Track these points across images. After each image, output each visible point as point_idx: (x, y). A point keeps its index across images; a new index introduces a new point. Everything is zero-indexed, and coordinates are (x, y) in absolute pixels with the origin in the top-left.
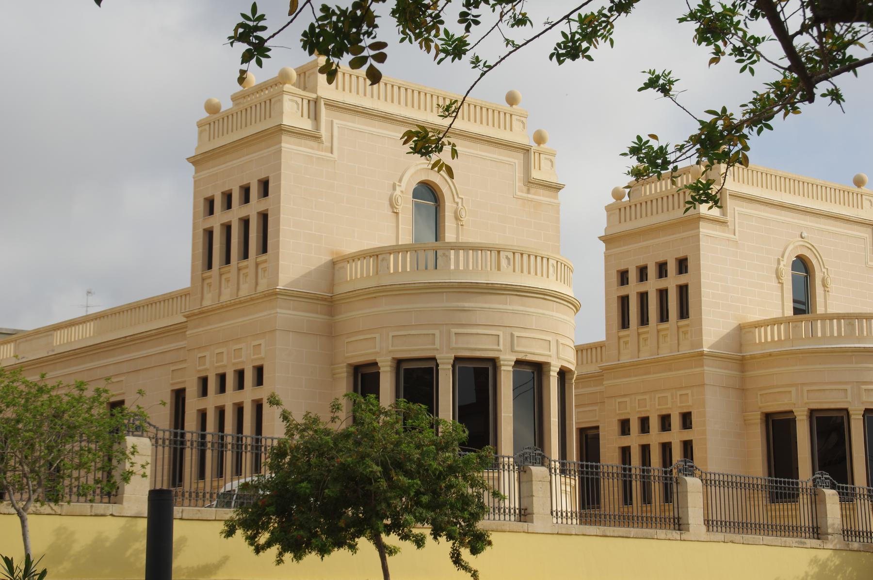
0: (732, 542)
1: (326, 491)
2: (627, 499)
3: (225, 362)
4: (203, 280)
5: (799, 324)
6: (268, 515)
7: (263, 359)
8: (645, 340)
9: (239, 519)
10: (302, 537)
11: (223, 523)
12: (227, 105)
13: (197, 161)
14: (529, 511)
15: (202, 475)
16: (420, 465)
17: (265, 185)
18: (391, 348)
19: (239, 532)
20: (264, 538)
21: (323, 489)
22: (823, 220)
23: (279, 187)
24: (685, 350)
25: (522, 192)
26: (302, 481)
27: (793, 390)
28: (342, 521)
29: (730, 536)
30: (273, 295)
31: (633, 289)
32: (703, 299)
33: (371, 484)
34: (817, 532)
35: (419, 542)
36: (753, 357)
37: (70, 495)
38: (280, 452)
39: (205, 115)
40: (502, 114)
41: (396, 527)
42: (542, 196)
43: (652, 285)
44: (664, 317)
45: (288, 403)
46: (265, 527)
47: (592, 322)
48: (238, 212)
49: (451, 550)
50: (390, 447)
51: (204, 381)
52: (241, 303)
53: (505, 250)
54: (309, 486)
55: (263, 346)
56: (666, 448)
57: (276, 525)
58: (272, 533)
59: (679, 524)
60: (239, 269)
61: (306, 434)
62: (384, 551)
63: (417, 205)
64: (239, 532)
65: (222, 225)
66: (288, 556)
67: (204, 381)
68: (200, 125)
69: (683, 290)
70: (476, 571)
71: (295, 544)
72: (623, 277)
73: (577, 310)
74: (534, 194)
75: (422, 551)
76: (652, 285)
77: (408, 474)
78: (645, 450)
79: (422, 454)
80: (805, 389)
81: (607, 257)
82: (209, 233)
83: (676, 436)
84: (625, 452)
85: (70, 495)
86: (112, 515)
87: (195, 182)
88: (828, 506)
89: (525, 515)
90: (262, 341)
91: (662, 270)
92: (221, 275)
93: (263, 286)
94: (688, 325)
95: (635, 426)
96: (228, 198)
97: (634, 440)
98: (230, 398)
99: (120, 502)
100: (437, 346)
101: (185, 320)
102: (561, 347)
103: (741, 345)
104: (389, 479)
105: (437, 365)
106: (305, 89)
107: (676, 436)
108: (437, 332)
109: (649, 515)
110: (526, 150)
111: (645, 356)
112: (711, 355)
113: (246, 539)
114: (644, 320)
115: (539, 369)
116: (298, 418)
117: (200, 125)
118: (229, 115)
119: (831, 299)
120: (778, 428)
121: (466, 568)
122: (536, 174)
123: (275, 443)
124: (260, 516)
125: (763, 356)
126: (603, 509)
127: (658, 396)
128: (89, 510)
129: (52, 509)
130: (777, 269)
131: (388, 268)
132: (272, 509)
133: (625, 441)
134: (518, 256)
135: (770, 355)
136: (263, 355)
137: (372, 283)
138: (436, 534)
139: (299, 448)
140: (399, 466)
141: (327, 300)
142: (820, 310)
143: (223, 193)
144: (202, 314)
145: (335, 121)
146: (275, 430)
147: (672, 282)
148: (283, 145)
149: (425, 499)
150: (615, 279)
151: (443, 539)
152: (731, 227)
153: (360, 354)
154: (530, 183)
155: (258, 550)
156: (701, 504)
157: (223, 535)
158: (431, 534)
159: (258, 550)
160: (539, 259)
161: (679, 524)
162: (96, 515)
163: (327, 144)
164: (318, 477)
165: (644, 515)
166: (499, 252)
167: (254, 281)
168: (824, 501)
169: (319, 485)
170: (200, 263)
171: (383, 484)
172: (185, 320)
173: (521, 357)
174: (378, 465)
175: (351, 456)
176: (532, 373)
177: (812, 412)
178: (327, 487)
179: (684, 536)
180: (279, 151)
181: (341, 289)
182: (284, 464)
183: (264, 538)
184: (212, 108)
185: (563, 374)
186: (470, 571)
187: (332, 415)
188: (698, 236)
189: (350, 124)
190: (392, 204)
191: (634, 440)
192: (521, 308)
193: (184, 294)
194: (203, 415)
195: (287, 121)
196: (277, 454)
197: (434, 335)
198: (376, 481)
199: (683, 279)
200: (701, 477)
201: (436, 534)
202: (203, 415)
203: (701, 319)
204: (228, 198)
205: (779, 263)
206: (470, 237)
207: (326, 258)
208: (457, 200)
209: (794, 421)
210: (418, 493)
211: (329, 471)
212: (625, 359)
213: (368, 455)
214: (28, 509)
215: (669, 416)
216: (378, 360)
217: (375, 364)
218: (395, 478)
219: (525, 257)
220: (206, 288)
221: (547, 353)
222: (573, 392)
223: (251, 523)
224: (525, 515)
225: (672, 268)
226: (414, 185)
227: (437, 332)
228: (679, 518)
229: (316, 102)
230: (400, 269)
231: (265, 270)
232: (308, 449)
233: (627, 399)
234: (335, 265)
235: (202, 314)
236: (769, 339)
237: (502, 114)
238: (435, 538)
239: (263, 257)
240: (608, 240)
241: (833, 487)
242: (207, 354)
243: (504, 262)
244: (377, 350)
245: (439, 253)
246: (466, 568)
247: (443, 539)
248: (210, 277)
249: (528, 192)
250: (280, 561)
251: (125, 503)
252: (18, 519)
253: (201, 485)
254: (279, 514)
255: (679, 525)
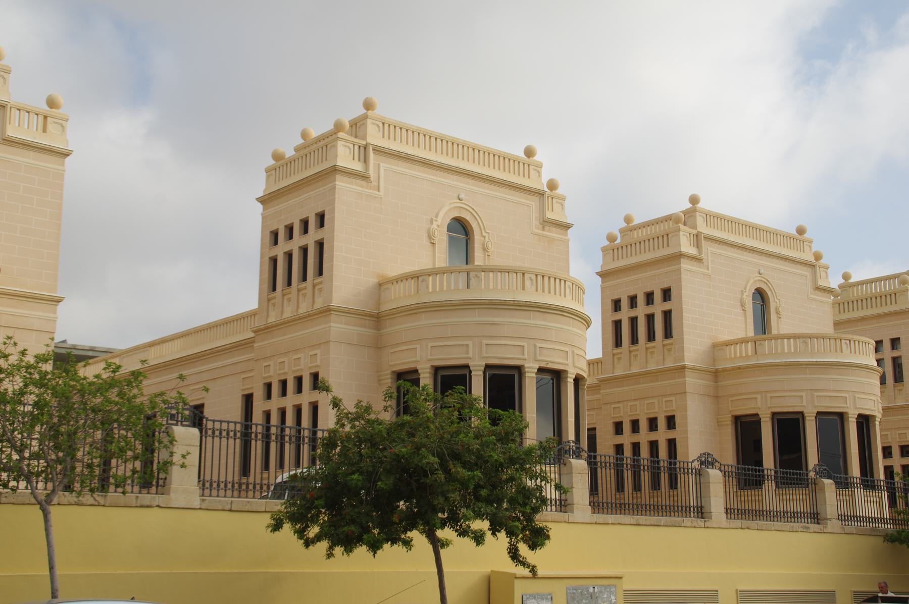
0: (748, 528)
1: (379, 483)
2: (620, 487)
3: (286, 370)
4: (269, 300)
5: (763, 342)
6: (316, 507)
7: (318, 366)
8: (636, 356)
9: (287, 512)
10: (353, 532)
11: (268, 516)
12: (289, 153)
13: (263, 200)
14: (569, 502)
15: (266, 466)
16: (479, 456)
17: (321, 218)
18: (430, 357)
19: (287, 527)
20: (314, 531)
21: (375, 482)
22: (775, 260)
23: (333, 218)
24: (669, 364)
25: (538, 229)
26: (353, 473)
27: (759, 396)
28: (396, 516)
29: (746, 523)
30: (327, 311)
31: (625, 315)
32: (684, 322)
33: (427, 476)
34: (816, 517)
35: (479, 538)
36: (724, 370)
37: (132, 486)
38: (331, 442)
39: (272, 162)
40: (521, 164)
41: (453, 520)
42: (554, 233)
43: (641, 311)
44: (651, 337)
45: (337, 391)
46: (314, 520)
47: (593, 343)
48: (299, 240)
49: (508, 545)
50: (447, 436)
51: (269, 386)
52: (300, 318)
53: (529, 272)
54: (361, 478)
55: (318, 356)
56: (654, 445)
57: (326, 518)
58: (321, 528)
59: (701, 512)
60: (299, 290)
61: (357, 423)
62: (437, 544)
63: (450, 237)
64: (287, 527)
65: (285, 253)
66: (338, 550)
67: (269, 386)
68: (268, 171)
69: (667, 315)
70: (534, 567)
71: (344, 537)
72: (617, 305)
73: (589, 326)
74: (549, 231)
75: (481, 548)
76: (641, 311)
77: (464, 465)
78: (636, 447)
79: (482, 445)
80: (769, 395)
81: (603, 289)
82: (274, 261)
83: (662, 435)
84: (619, 448)
85: (132, 486)
86: (158, 506)
87: (263, 218)
88: (827, 494)
89: (565, 506)
90: (318, 351)
91: (649, 298)
92: (283, 295)
93: (319, 304)
94: (672, 344)
95: (627, 427)
96: (290, 230)
97: (627, 439)
98: (290, 402)
99: (168, 493)
100: (470, 355)
101: (252, 335)
102: (576, 357)
103: (714, 360)
104: (447, 471)
105: (470, 372)
106: (356, 137)
107: (662, 435)
108: (470, 343)
109: (622, 501)
110: (541, 194)
111: (635, 370)
112: (693, 369)
113: (295, 532)
114: (634, 340)
115: (557, 376)
116: (349, 406)
117: (268, 171)
118: (292, 161)
119: (780, 325)
120: (746, 429)
121: (524, 564)
122: (550, 215)
123: (326, 434)
124: (309, 509)
125: (733, 369)
126: (600, 495)
127: (646, 402)
128: (134, 501)
129: (95, 499)
130: (741, 299)
131: (427, 288)
132: (321, 502)
133: (619, 440)
134: (540, 278)
135: (739, 368)
136: (318, 363)
137: (414, 301)
138: (494, 530)
139: (350, 438)
140: (456, 457)
141: (376, 319)
142: (774, 331)
143: (286, 226)
144: (266, 330)
145: (382, 164)
146: (328, 420)
147: (658, 308)
148: (337, 183)
149: (484, 492)
150: (610, 306)
151: (502, 535)
152: (705, 264)
153: (403, 363)
154: (546, 223)
155: (308, 543)
156: (722, 494)
157: (270, 529)
158: (489, 529)
159: (308, 543)
160: (558, 281)
161: (701, 512)
162: (142, 506)
163: (375, 183)
164: (370, 469)
165: (618, 501)
166: (524, 274)
167: (311, 300)
168: (823, 490)
169: (371, 477)
170: (266, 286)
171: (441, 476)
172: (252, 335)
173: (543, 365)
174: (433, 455)
175: (405, 447)
176: (554, 377)
177: (774, 414)
178: (380, 480)
179: (707, 524)
180: (334, 188)
181: (386, 307)
182: (334, 455)
183: (314, 531)
184: (277, 157)
185: (578, 380)
186: (528, 566)
187: (385, 404)
188: (679, 270)
189: (394, 167)
190: (430, 237)
191: (627, 439)
192: (543, 323)
193: (252, 314)
194: (268, 415)
195: (341, 163)
196: (327, 444)
197: (467, 345)
198: (432, 474)
199: (667, 306)
200: (720, 469)
201: (494, 530)
202: (268, 415)
203: (683, 338)
204: (290, 230)
205: (743, 294)
206: (497, 260)
207: (373, 281)
208: (484, 234)
209: (758, 423)
210: (478, 487)
211: (382, 462)
212: (619, 372)
213: (424, 446)
214: (51, 501)
215: (656, 419)
216: (418, 367)
217: (416, 371)
218: (453, 470)
219: (546, 279)
220: (271, 307)
221: (565, 362)
222: (585, 398)
223: (300, 518)
224: (565, 506)
225: (658, 296)
226: (448, 221)
227: (470, 343)
228: (702, 507)
229: (365, 147)
230: (439, 290)
231: (320, 290)
232: (360, 439)
233: (620, 405)
234: (382, 285)
235: (266, 330)
236: (738, 355)
237: (521, 164)
238: (494, 534)
239: (320, 279)
240: (604, 275)
241: (829, 478)
242: (271, 363)
243: (528, 283)
244: (418, 358)
245: (472, 274)
246: (524, 564)
247: (502, 535)
248: (274, 298)
249: (543, 229)
250: (330, 555)
251: (172, 494)
252: (41, 512)
253: (265, 475)
254: (329, 507)
255: (702, 513)
